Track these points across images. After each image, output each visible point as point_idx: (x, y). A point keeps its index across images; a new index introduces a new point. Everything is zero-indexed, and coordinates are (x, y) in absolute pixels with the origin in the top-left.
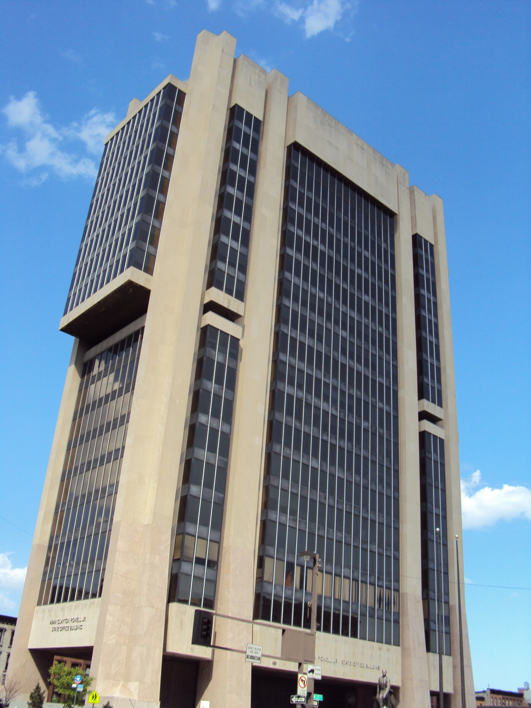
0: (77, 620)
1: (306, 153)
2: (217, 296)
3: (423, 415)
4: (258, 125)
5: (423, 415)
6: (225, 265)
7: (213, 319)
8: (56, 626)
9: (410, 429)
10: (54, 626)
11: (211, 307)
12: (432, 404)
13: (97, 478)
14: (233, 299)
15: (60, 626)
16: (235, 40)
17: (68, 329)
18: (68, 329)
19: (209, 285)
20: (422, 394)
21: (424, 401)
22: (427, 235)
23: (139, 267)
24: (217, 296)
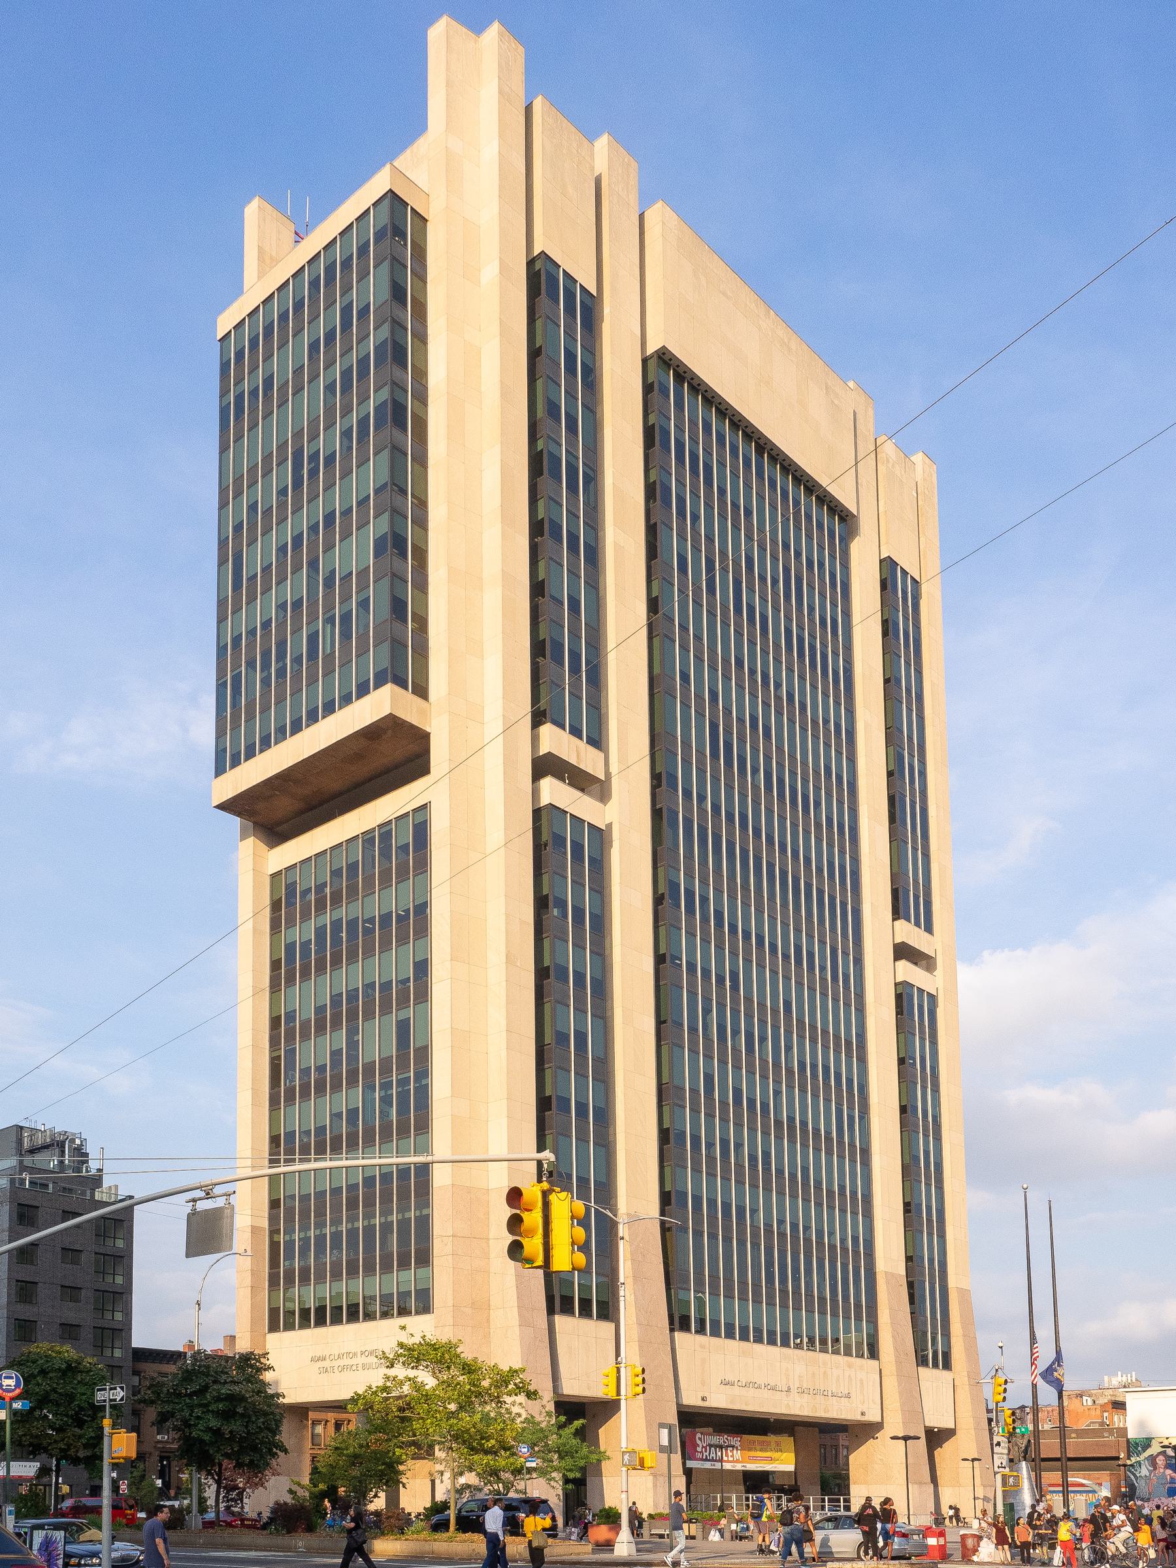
0: (515, 1223)
1: (683, 375)
2: (553, 739)
3: (903, 952)
4: (589, 311)
5: (903, 952)
6: (559, 669)
7: (553, 791)
8: (327, 1364)
9: (880, 976)
10: (321, 1364)
11: (545, 766)
12: (916, 929)
13: (424, 1082)
14: (582, 744)
15: (336, 1364)
16: (521, 49)
17: (609, 826)
18: (609, 826)
19: (538, 718)
20: (898, 912)
21: (901, 924)
22: (906, 561)
23: (401, 682)
24: (553, 739)
